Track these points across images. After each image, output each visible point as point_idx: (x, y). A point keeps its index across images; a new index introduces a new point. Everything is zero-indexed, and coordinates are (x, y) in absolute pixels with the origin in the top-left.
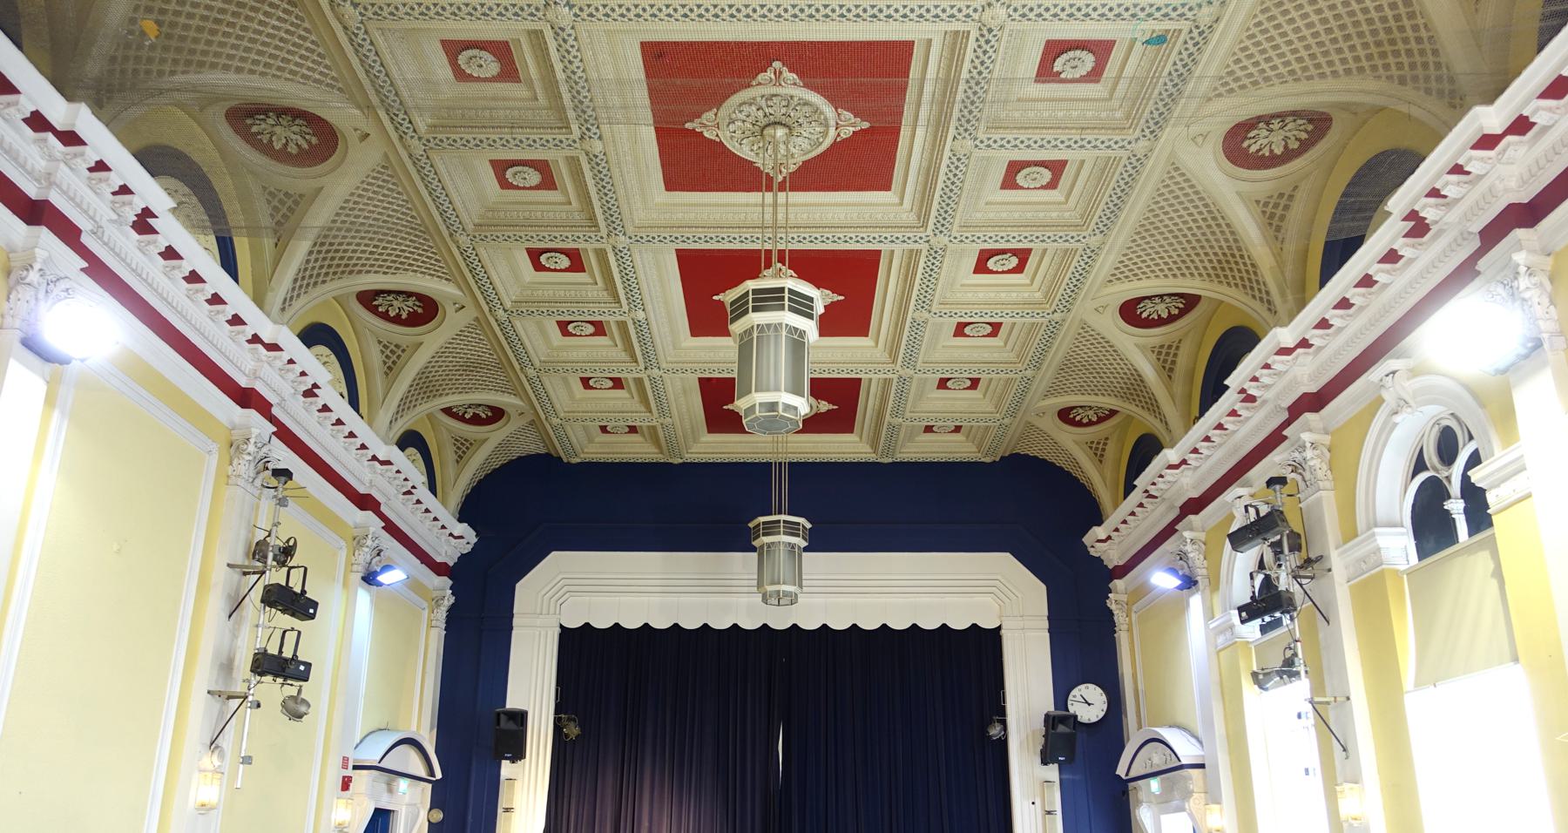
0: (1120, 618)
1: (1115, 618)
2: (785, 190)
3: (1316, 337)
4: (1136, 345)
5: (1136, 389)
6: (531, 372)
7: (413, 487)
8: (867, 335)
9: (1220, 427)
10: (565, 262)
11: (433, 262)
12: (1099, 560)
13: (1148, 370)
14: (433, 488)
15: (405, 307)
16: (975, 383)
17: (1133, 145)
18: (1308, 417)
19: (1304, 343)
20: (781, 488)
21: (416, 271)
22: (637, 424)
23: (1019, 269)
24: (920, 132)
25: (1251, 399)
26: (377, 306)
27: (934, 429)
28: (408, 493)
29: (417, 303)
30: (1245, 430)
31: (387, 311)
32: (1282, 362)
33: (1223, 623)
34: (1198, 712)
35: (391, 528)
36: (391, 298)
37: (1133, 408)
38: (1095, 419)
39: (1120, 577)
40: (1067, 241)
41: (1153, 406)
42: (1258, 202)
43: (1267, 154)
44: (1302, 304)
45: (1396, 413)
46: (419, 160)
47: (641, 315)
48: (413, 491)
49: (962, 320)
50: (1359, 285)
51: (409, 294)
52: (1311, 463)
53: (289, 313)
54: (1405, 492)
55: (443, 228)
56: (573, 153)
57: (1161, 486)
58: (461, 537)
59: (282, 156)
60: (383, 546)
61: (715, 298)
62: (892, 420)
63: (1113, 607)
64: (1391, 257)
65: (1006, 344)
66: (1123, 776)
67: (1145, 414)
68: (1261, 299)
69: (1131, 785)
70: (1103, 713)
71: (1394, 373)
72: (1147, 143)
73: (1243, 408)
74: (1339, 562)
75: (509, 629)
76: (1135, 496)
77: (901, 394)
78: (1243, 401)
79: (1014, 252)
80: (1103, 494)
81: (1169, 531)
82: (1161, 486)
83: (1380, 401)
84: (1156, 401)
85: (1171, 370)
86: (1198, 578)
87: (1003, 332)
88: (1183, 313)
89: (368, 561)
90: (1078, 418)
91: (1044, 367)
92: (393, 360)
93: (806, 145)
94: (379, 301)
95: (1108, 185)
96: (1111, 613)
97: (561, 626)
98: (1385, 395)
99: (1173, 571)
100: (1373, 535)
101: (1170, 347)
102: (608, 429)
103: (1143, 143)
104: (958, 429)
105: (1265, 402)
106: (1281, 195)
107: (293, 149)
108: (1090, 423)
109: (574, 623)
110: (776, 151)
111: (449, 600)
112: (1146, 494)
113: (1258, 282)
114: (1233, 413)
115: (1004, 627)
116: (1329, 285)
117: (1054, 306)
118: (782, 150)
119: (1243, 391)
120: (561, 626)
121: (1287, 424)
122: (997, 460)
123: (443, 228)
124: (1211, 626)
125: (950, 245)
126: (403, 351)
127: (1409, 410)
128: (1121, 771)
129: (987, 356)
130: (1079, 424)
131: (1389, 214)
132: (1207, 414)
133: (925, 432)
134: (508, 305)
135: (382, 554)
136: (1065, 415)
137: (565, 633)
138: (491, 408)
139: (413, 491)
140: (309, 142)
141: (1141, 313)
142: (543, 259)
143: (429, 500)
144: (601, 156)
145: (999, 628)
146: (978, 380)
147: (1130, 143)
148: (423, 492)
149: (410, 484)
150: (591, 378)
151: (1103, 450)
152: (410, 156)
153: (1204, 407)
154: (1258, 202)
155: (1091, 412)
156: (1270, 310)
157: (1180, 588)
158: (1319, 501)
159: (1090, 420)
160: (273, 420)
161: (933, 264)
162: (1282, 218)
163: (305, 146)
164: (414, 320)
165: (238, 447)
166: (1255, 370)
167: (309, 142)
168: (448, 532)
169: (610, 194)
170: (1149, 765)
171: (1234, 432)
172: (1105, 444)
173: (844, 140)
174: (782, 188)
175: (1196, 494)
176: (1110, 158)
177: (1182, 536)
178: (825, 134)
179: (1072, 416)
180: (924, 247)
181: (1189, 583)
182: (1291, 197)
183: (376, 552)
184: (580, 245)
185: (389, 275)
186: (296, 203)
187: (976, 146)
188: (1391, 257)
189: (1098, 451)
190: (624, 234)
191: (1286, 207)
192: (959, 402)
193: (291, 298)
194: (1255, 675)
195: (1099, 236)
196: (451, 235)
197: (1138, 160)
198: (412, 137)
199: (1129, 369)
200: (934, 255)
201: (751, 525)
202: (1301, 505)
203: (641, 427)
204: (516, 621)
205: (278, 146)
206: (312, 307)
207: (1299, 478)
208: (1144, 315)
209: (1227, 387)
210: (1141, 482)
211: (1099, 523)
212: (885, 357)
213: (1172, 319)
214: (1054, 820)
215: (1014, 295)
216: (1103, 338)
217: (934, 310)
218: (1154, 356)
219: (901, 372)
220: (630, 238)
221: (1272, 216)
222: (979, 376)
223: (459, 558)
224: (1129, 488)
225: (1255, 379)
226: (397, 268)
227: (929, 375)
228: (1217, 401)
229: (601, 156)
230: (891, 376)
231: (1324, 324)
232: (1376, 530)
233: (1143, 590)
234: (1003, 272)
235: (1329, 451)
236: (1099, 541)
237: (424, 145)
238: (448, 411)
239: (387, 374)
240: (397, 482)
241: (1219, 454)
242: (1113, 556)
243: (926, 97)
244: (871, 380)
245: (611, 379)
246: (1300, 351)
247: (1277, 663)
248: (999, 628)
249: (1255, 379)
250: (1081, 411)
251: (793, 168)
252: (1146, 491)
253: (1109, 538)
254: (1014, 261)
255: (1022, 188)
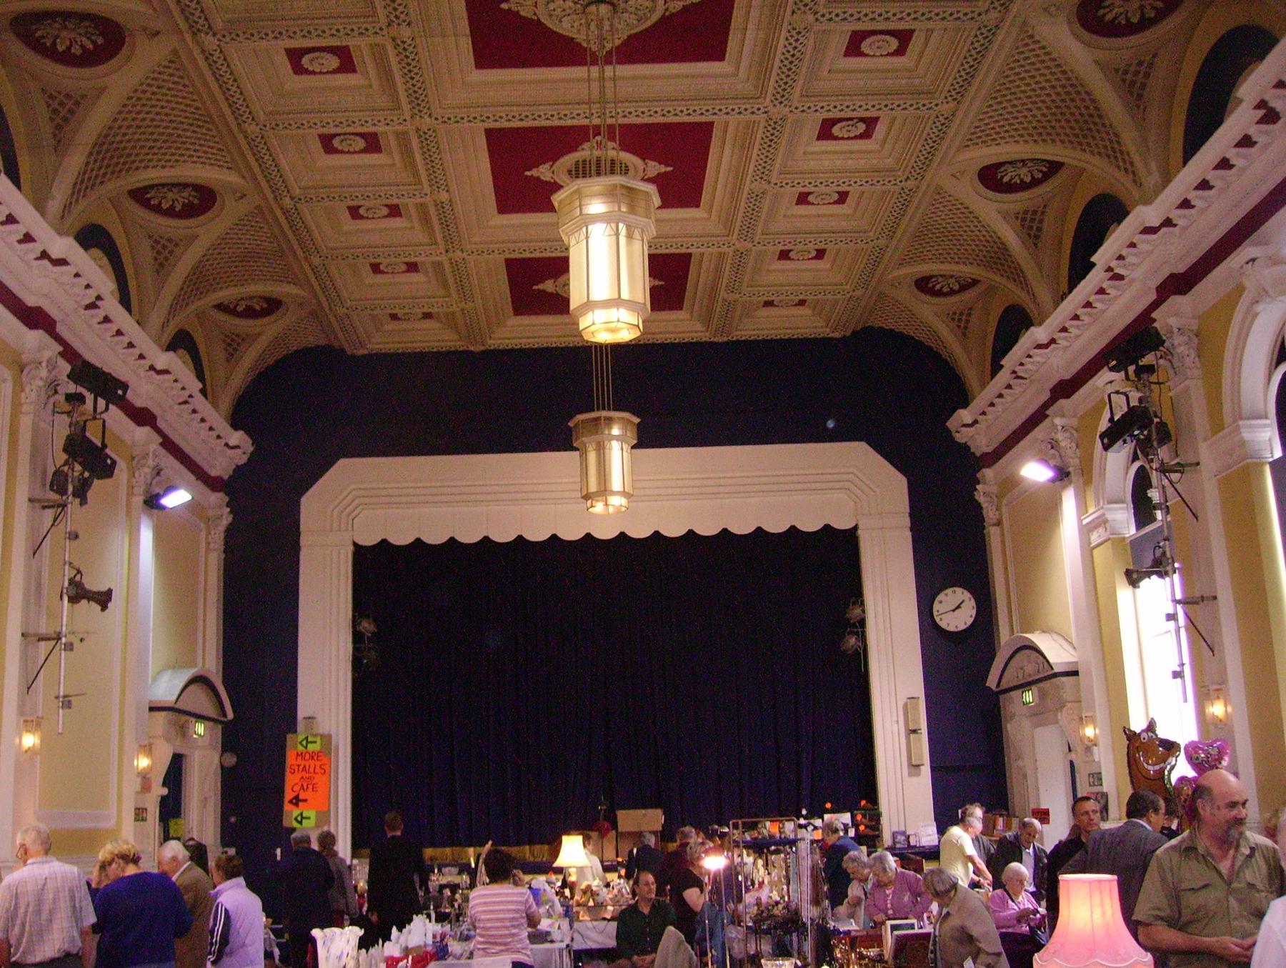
0: (990, 513)
1: (984, 512)
2: (611, 63)
3: (1177, 215)
4: (1097, 62)
5: (998, 257)
6: (316, 261)
7: (191, 396)
8: (698, 206)
9: (1088, 305)
10: (333, 62)
11: (215, 151)
12: (965, 447)
13: (1011, 237)
14: (125, 302)
15: (179, 199)
16: (842, 197)
17: (983, 16)
18: (1175, 301)
19: (1168, 223)
20: (603, 381)
21: (195, 162)
22: (434, 310)
23: (866, 135)
24: (727, 152)
25: (1118, 277)
26: (149, 200)
27: (792, 255)
28: (186, 402)
29: (193, 193)
30: (1114, 309)
31: (160, 203)
32: (1148, 242)
33: (1097, 518)
34: (1072, 615)
35: (169, 445)
36: (165, 190)
37: (998, 278)
38: (956, 287)
39: (989, 466)
40: (918, 108)
41: (1017, 275)
42: (1117, 70)
43: (1123, 22)
44: (1167, 178)
45: (1257, 302)
46: (212, 55)
47: (444, 196)
48: (190, 400)
49: (831, 115)
50: (1238, 145)
51: (186, 186)
52: (1179, 350)
53: (69, 221)
54: (1269, 383)
55: (231, 119)
56: (378, 39)
57: (1029, 367)
58: (166, 372)
59: (67, 59)
60: (163, 465)
61: (528, 173)
62: (726, 296)
63: (981, 499)
64: (1246, 142)
65: (855, 211)
66: (993, 687)
67: (1011, 285)
68: (1126, 170)
69: (1002, 697)
70: (972, 620)
71: (1253, 260)
72: (997, 15)
73: (1098, 300)
74: (1207, 454)
75: (296, 548)
76: (1003, 376)
77: (739, 267)
78: (1260, 122)
79: (862, 120)
80: (971, 374)
81: (1038, 417)
82: (1029, 367)
83: (1240, 289)
84: (1021, 270)
85: (1037, 237)
86: (1071, 469)
87: (880, 130)
88: (1046, 177)
89: (149, 482)
90: (938, 287)
91: (899, 234)
92: (164, 253)
93: (633, 20)
94: (152, 193)
95: (960, 54)
96: (979, 506)
97: (355, 544)
98: (1247, 283)
99: (1044, 461)
100: (1238, 428)
101: (1035, 212)
102: (382, 267)
103: (994, 15)
104: (802, 303)
105: (1133, 280)
106: (1140, 64)
107: (77, 50)
108: (952, 292)
109: (369, 540)
110: (600, 26)
111: (227, 519)
112: (1261, 112)
113: (1122, 152)
114: (1101, 291)
115: (860, 526)
116: (1191, 163)
117: (907, 173)
118: (606, 26)
119: (1109, 269)
120: (355, 544)
121: (1155, 305)
122: (848, 334)
123: (231, 119)
124: (1085, 522)
125: (789, 115)
126: (176, 245)
127: (1268, 299)
128: (992, 682)
129: (835, 224)
130: (940, 294)
131: (1241, 101)
132: (1074, 292)
133: (779, 259)
134: (297, 192)
135: (162, 473)
136: (924, 285)
137: (360, 553)
138: (198, 188)
139: (190, 400)
140: (94, 42)
141: (1002, 177)
142: (305, 61)
143: (122, 318)
144: (409, 42)
145: (856, 528)
146: (824, 250)
147: (937, 105)
148: (111, 305)
149: (187, 393)
150: (359, 207)
151: (967, 321)
152: (203, 51)
153: (1072, 285)
154: (1117, 70)
155: (953, 280)
156: (1135, 181)
157: (1053, 481)
158: (1187, 389)
159: (951, 289)
160: (159, 431)
161: (772, 135)
162: (1143, 86)
163: (91, 47)
164: (189, 211)
165: (139, 461)
166: (1028, 349)
167: (94, 42)
168: (147, 363)
169: (417, 78)
170: (1020, 677)
171: (1103, 311)
172: (969, 315)
173: (673, 14)
174: (608, 61)
175: (1067, 376)
176: (959, 29)
177: (1053, 424)
178: (652, 10)
179: (930, 285)
180: (761, 117)
181: (1062, 475)
182: (1151, 65)
183: (155, 472)
184: (380, 129)
185: (167, 169)
186: (77, 103)
187: (817, 20)
188: (1246, 142)
189: (961, 322)
190: (430, 116)
191: (1147, 75)
192: (803, 271)
193: (71, 203)
194: (1128, 573)
195: (953, 104)
196: (239, 124)
197: (989, 31)
198: (207, 34)
199: (991, 236)
200: (783, 86)
201: (571, 424)
202: (1171, 394)
203: (424, 263)
204: (304, 540)
205: (61, 48)
206: (85, 213)
207: (1168, 364)
208: (1006, 179)
209: (1093, 265)
210: (1009, 361)
211: (965, 404)
212: (720, 230)
213: (1035, 183)
214: (920, 740)
215: (862, 162)
216: (962, 204)
217: (774, 181)
218: (1018, 223)
219: (738, 246)
220: (436, 119)
221: (1132, 84)
222: (826, 247)
223: (234, 470)
224: (996, 368)
225: (1121, 258)
226: (177, 161)
227: (770, 247)
228: (1084, 277)
229: (409, 42)
230: (725, 249)
231: (1224, 164)
232: (1241, 423)
233: (1011, 482)
234: (849, 138)
235: (1197, 336)
236: (964, 425)
237: (219, 40)
238: (140, 196)
239: (158, 272)
240: (174, 392)
241: (1088, 334)
242: (981, 442)
243: (724, 167)
244: (702, 255)
245: (362, 135)
246: (1164, 230)
247: (1148, 560)
248: (856, 528)
249: (1121, 258)
250: (940, 279)
251: (617, 42)
252: (1014, 372)
253: (975, 422)
254: (862, 127)
255: (867, 55)
